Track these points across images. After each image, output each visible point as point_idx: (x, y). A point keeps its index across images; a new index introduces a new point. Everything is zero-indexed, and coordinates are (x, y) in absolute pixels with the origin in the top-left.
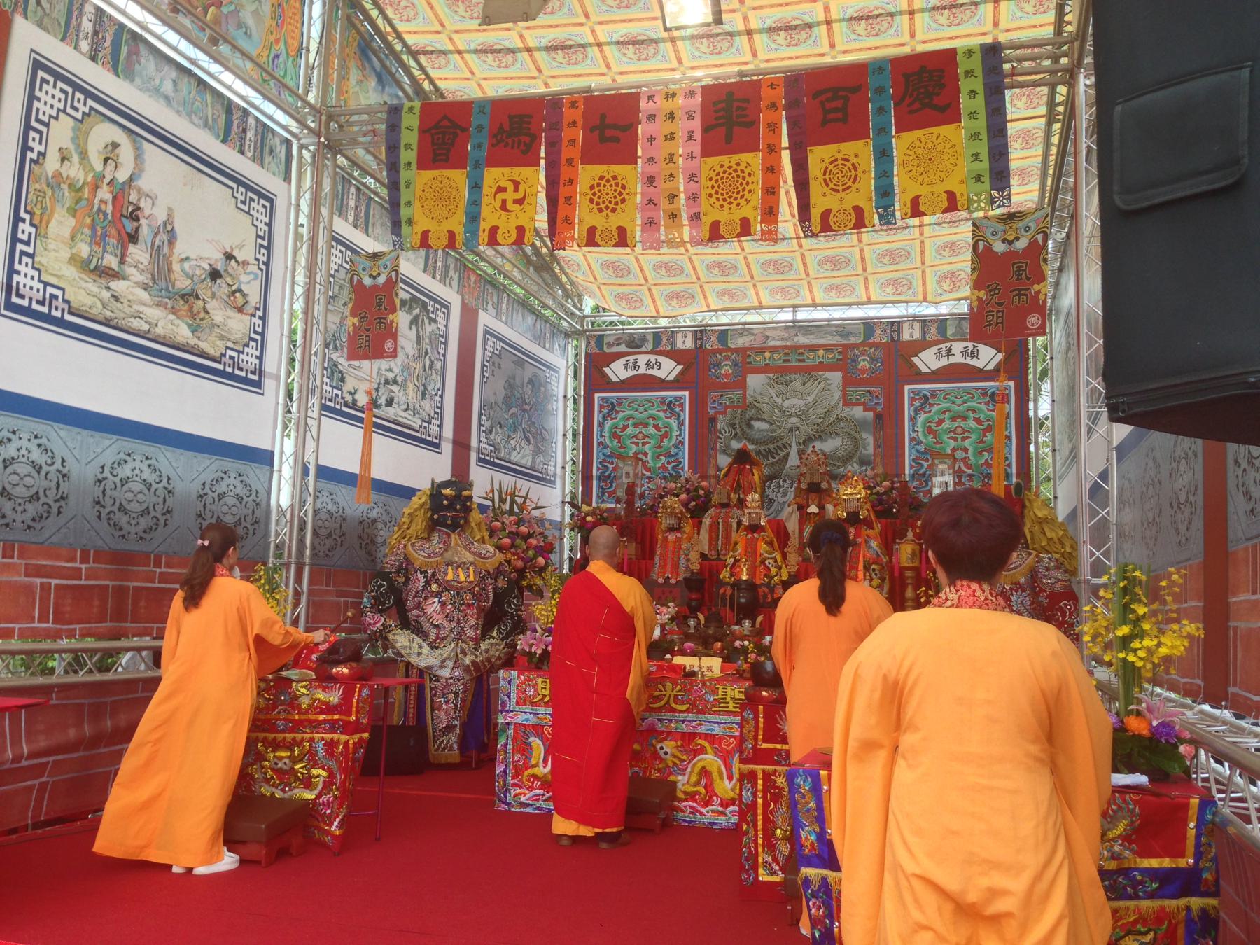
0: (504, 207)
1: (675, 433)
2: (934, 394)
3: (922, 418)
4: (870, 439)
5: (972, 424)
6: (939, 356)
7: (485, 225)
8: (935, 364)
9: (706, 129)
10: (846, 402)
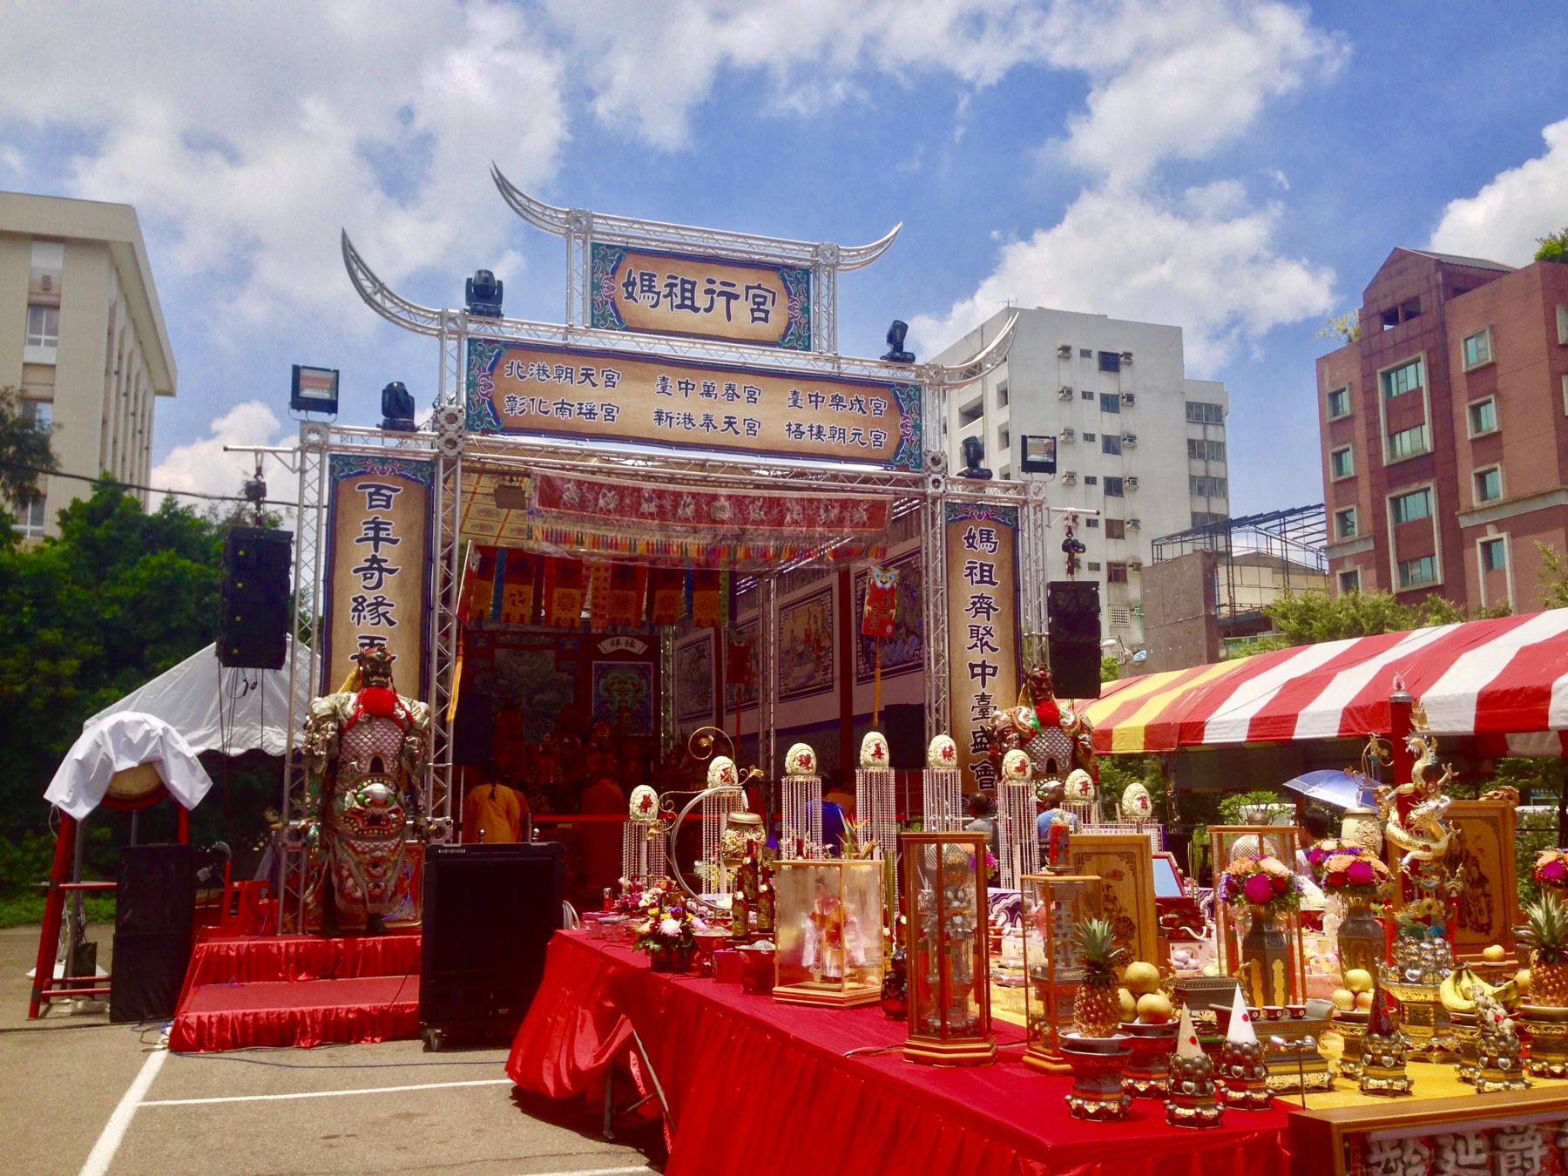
0: (513, 603)
1: (645, 688)
2: (609, 666)
3: (602, 681)
4: (571, 693)
5: (629, 686)
6: (612, 644)
7: (504, 612)
8: (612, 649)
9: (613, 577)
10: (558, 669)
